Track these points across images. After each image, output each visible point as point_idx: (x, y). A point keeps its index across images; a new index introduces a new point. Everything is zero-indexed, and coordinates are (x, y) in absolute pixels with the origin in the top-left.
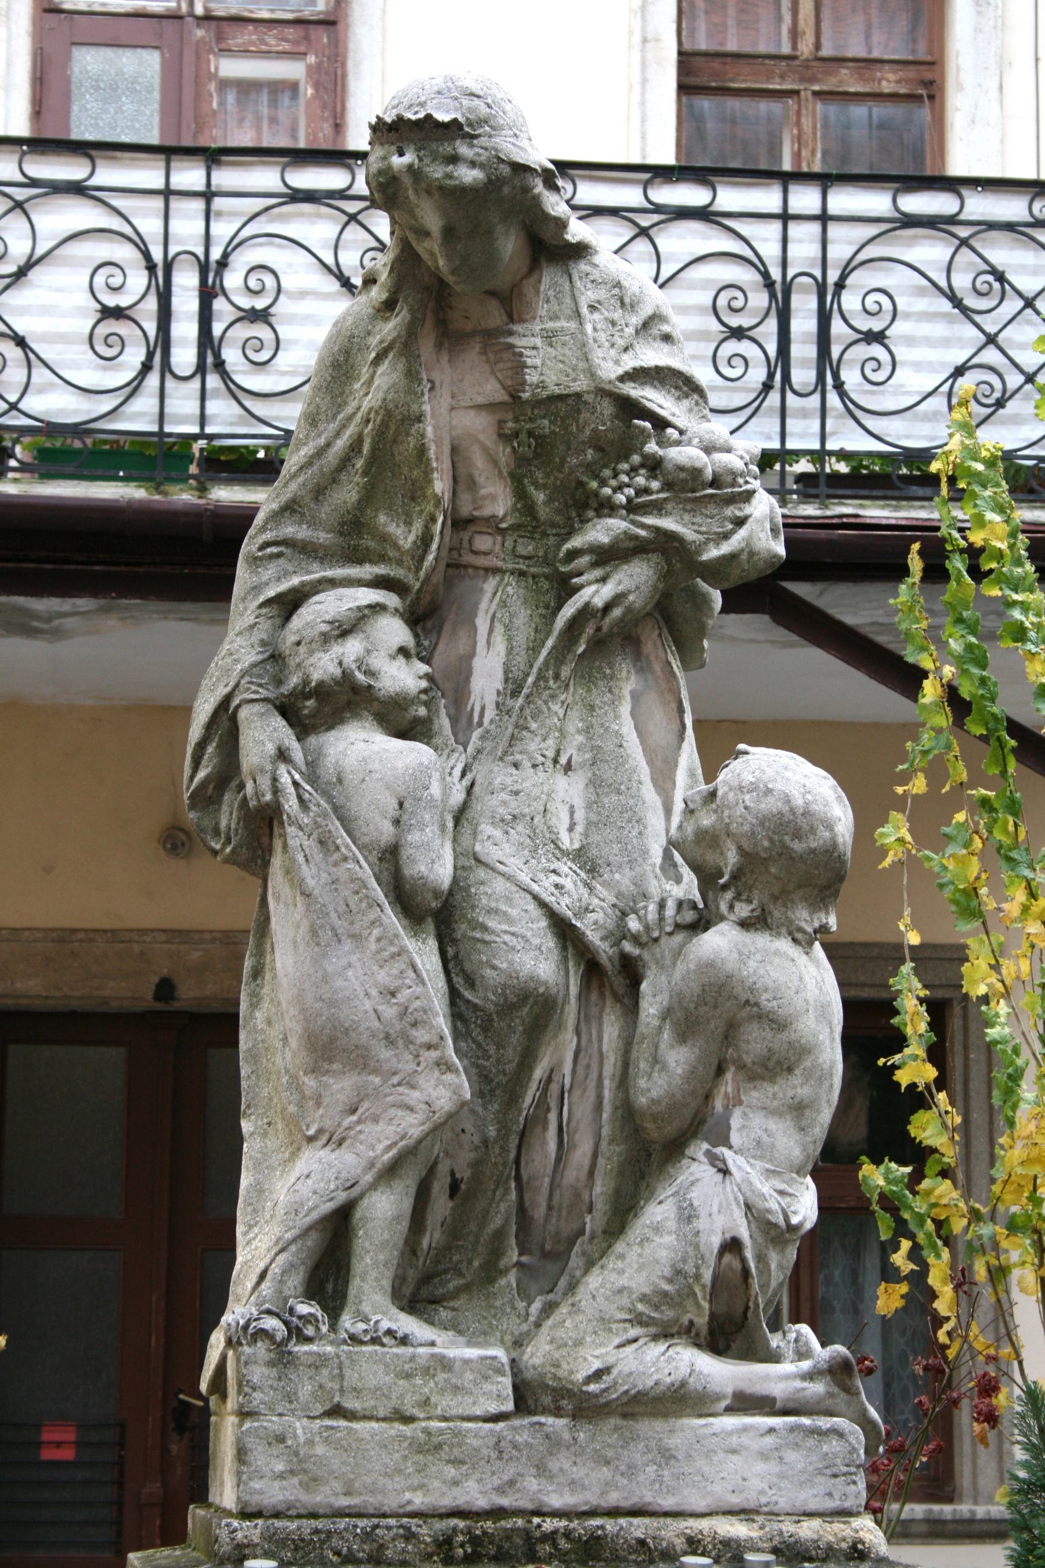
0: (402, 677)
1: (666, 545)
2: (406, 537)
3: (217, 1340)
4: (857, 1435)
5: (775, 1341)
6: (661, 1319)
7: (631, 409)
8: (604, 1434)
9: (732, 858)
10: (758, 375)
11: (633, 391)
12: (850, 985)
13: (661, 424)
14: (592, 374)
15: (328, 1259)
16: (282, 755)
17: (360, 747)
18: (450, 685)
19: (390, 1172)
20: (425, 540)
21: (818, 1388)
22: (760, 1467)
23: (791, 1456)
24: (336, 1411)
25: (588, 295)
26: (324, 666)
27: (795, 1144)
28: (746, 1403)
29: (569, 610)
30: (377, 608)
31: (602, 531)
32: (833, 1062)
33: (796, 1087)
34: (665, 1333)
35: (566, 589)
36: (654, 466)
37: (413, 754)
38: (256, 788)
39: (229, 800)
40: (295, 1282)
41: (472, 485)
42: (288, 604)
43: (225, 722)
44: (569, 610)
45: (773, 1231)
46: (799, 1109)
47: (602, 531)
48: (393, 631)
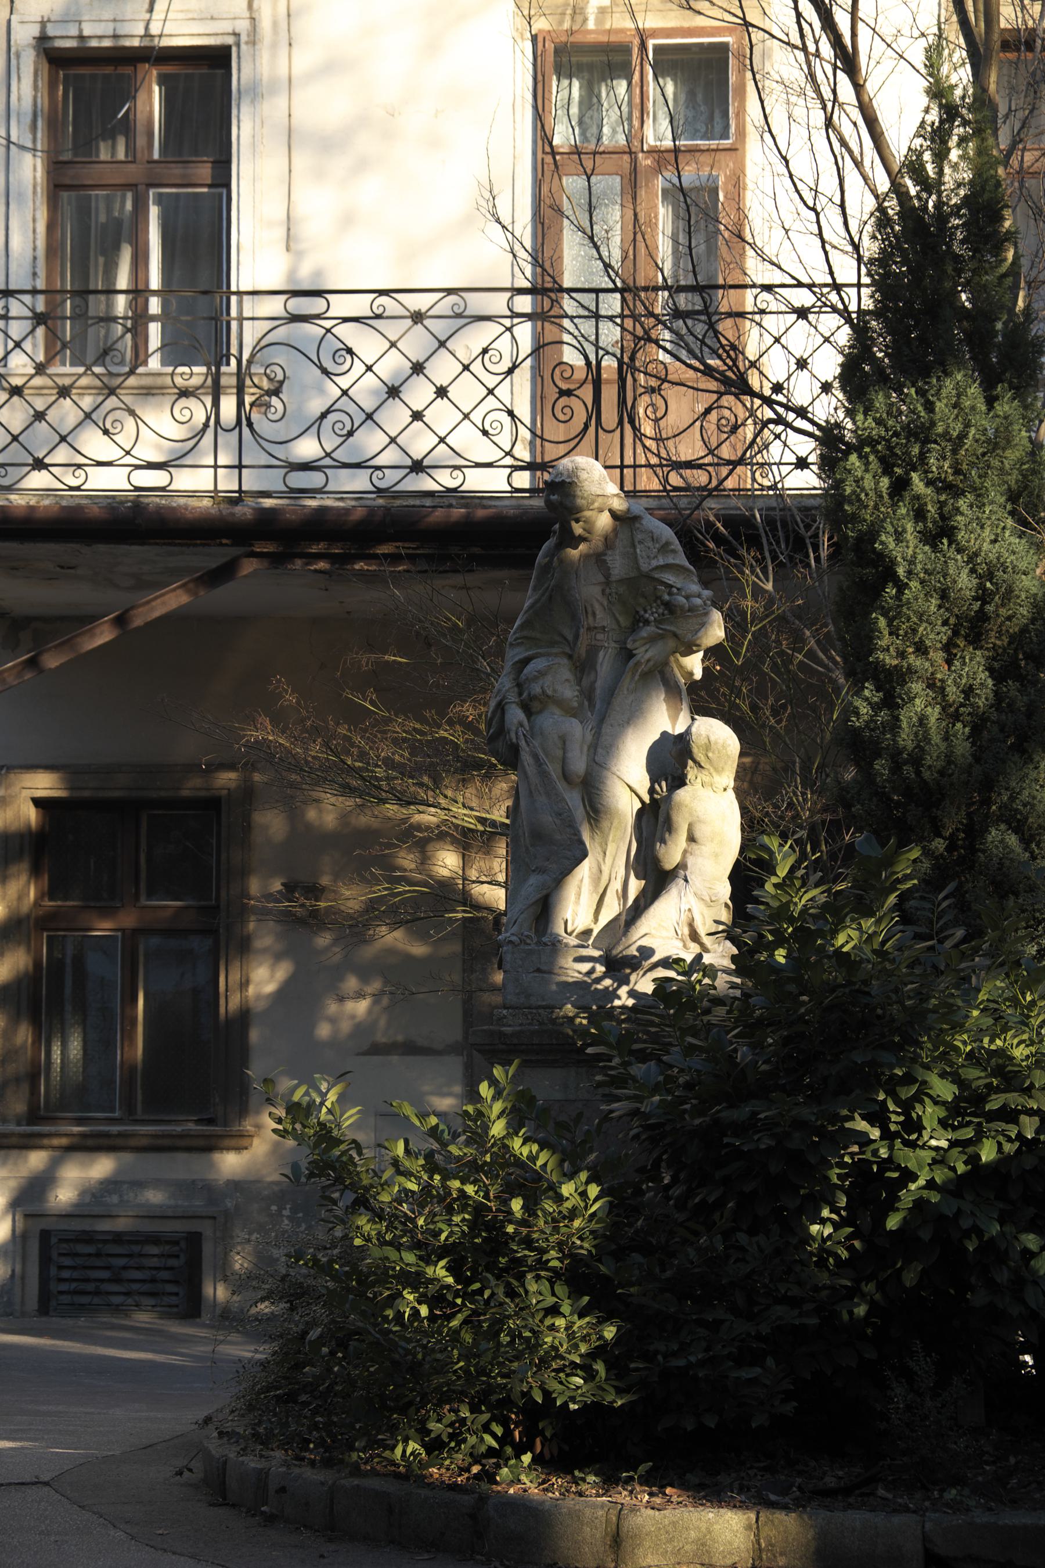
10: (581, 416)
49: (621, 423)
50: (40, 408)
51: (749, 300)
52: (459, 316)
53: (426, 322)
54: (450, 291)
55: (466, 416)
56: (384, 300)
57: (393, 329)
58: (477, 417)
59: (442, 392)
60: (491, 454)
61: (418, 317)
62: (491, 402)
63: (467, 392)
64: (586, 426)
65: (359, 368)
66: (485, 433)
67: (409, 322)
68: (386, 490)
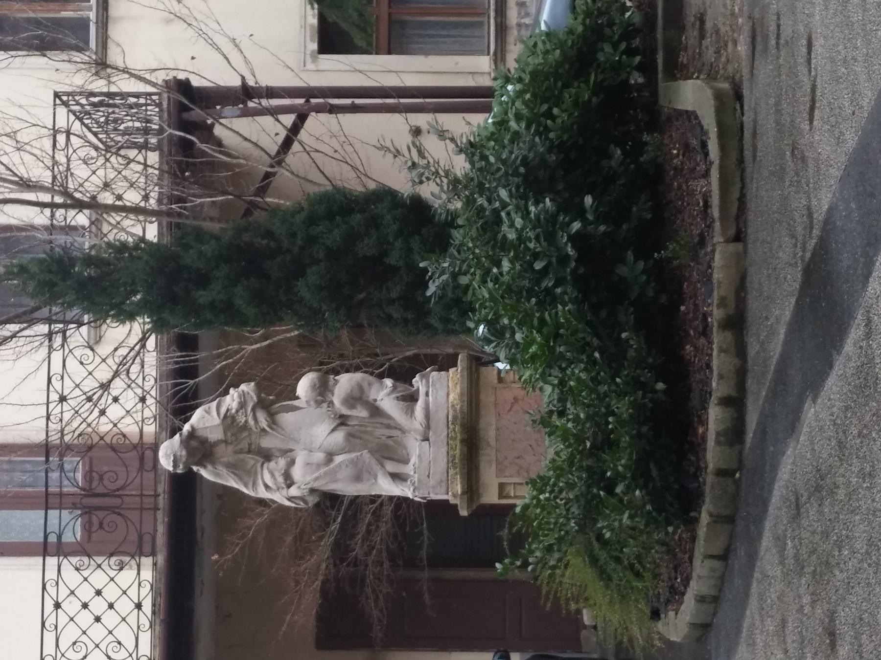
0: (282, 462)
1: (254, 410)
2: (252, 462)
3: (416, 499)
4: (434, 373)
5: (415, 388)
6: (410, 412)
7: (225, 416)
8: (432, 425)
9: (319, 398)
10: (114, 517)
11: (222, 416)
12: (140, 546)
13: (228, 410)
14: (219, 425)
15: (396, 477)
16: (299, 487)
17: (297, 473)
18: (285, 452)
19: (382, 466)
20: (253, 458)
21: (424, 381)
22: (696, 232)
23: (437, 387)
24: (428, 476)
25: (201, 426)
26: (280, 479)
27: (376, 386)
28: (427, 394)
29: (268, 429)
30: (268, 468)
31: (251, 422)
32: (227, 481)
33: (365, 385)
34: (413, 412)
35: (263, 430)
36: (237, 411)
37: (299, 461)
38: (306, 492)
39: (307, 498)
40: (404, 484)
41: (241, 449)
42: (267, 487)
43: (290, 499)
44: (268, 429)
45: (395, 388)
46: (370, 384)
47: (251, 422)
48: (272, 464)
49: (119, 496)
50: (99, 563)
51: (54, 426)
52: (57, 583)
53: (136, 610)
54: (44, 587)
55: (84, 633)
56: (47, 625)
57: (63, 619)
58: (84, 638)
59: (99, 593)
60: (63, 646)
61: (57, 606)
62: (91, 646)
63: (97, 632)
64: (119, 514)
65: (112, 574)
66: (74, 643)
67: (59, 610)
68: (151, 623)
